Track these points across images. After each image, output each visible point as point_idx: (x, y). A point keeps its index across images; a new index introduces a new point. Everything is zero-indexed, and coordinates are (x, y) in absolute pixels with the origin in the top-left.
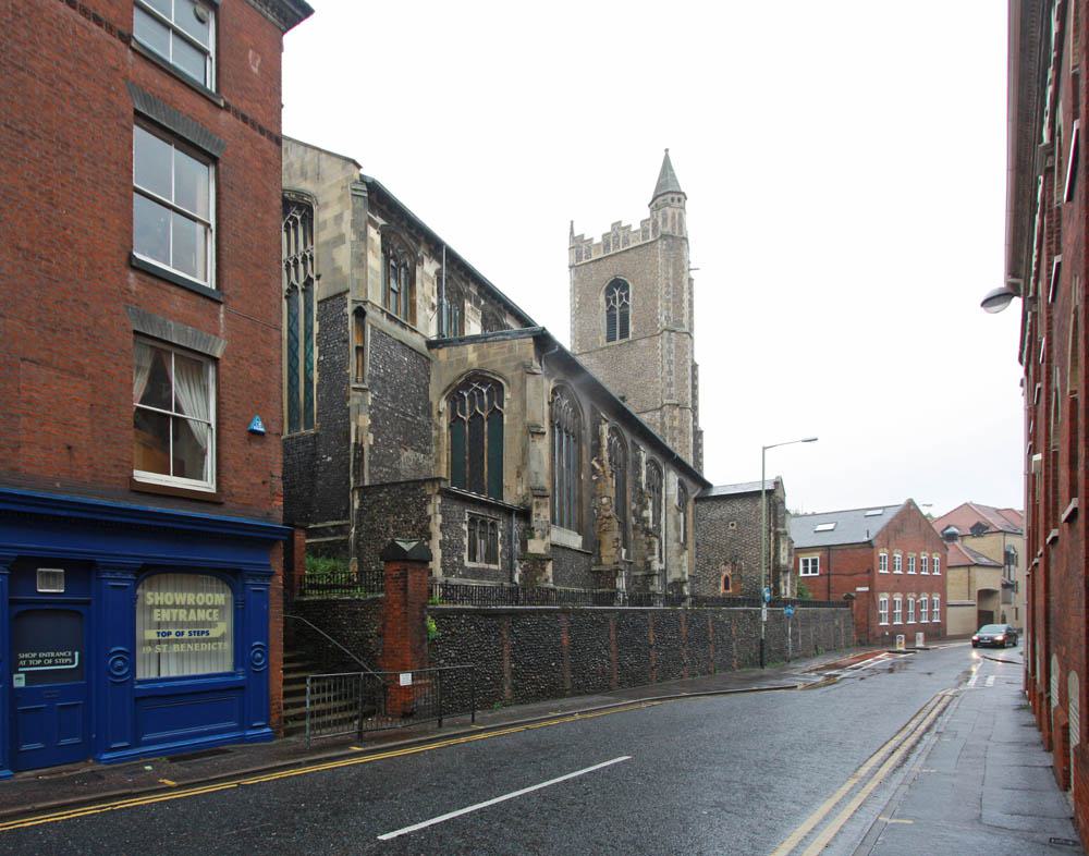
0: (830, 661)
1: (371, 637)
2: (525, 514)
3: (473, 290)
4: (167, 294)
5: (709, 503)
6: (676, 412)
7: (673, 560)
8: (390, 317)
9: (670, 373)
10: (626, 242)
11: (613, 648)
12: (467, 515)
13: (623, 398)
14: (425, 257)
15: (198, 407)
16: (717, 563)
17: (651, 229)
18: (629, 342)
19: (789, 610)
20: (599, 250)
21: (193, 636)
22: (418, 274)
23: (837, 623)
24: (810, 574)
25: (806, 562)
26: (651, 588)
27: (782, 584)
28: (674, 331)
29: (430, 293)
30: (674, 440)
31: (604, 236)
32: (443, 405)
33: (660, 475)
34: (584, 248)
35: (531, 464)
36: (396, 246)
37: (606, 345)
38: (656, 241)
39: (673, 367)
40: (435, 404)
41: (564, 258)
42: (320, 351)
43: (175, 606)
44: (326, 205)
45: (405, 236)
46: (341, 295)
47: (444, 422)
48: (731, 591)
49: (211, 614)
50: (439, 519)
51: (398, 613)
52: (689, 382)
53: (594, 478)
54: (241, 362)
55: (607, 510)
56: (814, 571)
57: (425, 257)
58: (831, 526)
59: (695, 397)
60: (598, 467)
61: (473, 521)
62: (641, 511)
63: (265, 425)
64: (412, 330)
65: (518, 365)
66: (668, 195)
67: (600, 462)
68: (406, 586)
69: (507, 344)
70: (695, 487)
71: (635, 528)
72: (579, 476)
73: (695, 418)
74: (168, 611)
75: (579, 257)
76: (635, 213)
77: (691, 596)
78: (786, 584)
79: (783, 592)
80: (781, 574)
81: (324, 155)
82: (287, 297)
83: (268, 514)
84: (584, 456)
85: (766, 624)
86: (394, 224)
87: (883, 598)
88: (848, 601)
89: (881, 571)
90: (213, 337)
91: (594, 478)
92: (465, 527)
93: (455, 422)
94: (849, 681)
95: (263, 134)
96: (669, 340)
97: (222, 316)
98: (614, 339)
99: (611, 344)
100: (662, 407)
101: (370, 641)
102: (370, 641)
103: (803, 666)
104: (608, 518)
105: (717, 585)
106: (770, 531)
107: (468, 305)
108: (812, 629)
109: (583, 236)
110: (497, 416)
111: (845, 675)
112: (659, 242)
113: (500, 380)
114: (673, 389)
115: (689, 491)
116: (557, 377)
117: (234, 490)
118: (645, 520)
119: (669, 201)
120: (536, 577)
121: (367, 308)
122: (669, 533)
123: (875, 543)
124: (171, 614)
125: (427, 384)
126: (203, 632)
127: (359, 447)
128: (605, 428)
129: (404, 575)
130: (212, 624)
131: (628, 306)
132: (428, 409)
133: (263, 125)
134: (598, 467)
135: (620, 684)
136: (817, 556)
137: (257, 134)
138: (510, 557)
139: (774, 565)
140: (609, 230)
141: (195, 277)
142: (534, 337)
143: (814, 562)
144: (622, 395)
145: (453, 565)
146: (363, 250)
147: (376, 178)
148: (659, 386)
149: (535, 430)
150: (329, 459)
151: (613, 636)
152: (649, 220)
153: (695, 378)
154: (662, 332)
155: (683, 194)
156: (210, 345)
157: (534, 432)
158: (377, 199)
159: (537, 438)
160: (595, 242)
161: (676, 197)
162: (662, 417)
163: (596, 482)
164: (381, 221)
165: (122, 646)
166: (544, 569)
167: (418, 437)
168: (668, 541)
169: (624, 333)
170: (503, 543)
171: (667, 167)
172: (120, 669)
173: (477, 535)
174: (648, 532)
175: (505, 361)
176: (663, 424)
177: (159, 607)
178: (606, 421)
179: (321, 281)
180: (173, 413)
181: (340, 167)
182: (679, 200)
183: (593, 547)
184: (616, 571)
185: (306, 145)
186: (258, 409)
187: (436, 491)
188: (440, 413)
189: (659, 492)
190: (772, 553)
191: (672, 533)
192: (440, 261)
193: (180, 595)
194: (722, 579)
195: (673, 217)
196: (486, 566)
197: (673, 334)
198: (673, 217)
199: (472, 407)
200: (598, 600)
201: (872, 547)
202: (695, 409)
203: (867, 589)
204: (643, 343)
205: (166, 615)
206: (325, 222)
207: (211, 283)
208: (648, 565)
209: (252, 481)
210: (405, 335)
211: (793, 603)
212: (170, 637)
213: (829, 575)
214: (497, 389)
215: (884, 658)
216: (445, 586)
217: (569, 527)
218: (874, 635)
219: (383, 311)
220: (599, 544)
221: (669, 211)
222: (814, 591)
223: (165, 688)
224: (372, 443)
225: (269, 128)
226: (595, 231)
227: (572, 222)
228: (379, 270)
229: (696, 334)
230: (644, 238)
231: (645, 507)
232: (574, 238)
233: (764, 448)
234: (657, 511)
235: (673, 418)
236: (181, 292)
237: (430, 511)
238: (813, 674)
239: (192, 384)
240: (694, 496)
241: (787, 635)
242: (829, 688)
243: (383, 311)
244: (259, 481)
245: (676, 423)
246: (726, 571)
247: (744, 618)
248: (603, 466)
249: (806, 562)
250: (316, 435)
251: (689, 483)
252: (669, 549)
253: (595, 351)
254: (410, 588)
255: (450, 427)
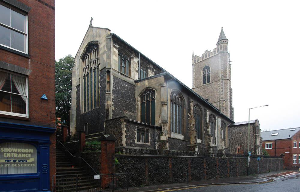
0: (273, 174)
1: (98, 164)
2: (160, 129)
3: (152, 67)
4: (7, 55)
5: (233, 127)
6: (224, 102)
7: (219, 144)
8: (121, 74)
9: (222, 91)
10: (209, 55)
11: (189, 168)
12: (136, 128)
13: (207, 100)
14: (134, 57)
15: (24, 92)
16: (235, 145)
17: (217, 50)
18: (210, 83)
19: (259, 159)
20: (201, 59)
21: (20, 162)
22: (132, 61)
23: (277, 163)
24: (269, 148)
25: (267, 145)
26: (210, 152)
27: (257, 151)
28: (224, 79)
29: (136, 68)
30: (223, 110)
31: (202, 55)
32: (139, 99)
33: (215, 119)
34: (197, 58)
35: (165, 113)
36: (124, 54)
37: (203, 85)
38: (218, 54)
39: (223, 90)
40: (137, 98)
41: (191, 62)
42: (100, 85)
43: (12, 152)
44: (102, 43)
45: (127, 51)
46: (105, 68)
47: (139, 104)
48: (240, 153)
49: (28, 155)
50: (125, 129)
51: (104, 157)
52: (229, 94)
53: (188, 119)
54: (38, 77)
55: (192, 128)
56: (270, 147)
57: (134, 57)
58: (277, 134)
59: (231, 98)
60: (189, 115)
61: (139, 130)
62: (207, 129)
63: (47, 97)
64: (129, 78)
65: (159, 85)
66: (223, 40)
67: (190, 114)
68: (106, 148)
69: (156, 79)
70: (228, 123)
71: (205, 134)
72: (183, 119)
73: (231, 104)
74: (10, 154)
75: (195, 62)
76: (212, 46)
77: (226, 154)
78: (258, 151)
79: (258, 153)
80: (257, 148)
81: (101, 30)
82: (93, 71)
83: (49, 125)
84: (185, 112)
85: (249, 162)
86: (123, 47)
87: (295, 155)
88: (282, 156)
89: (294, 147)
90: (26, 69)
91: (188, 119)
92: (136, 132)
93: (142, 104)
94: (278, 181)
95: (47, 6)
96: (222, 82)
97: (30, 62)
98: (205, 83)
99: (204, 85)
100: (220, 101)
101: (98, 165)
102: (98, 165)
103: (263, 176)
104: (192, 130)
105: (236, 151)
106: (253, 135)
107: (149, 71)
108: (268, 164)
109: (196, 55)
110: (153, 100)
111: (277, 179)
112: (219, 54)
113: (154, 90)
114: (223, 96)
115: (226, 124)
116: (173, 88)
117: (35, 117)
118: (208, 131)
119: (223, 42)
120: (163, 147)
121: (112, 71)
122: (218, 136)
123: (292, 139)
124: (11, 155)
125: (134, 93)
126: (24, 161)
127: (108, 110)
128: (192, 104)
129: (106, 145)
130: (29, 158)
131: (210, 74)
132: (134, 100)
133: (46, 3)
134: (189, 115)
135: (192, 180)
136: (271, 143)
137: (45, 6)
138: (154, 141)
139: (255, 145)
140: (204, 53)
141: (24, 52)
142: (164, 76)
143: (270, 145)
144: (207, 98)
145: (131, 143)
146: (110, 54)
147: (115, 33)
148: (219, 95)
149: (164, 103)
150: (102, 114)
151: (189, 165)
152: (216, 48)
153: (231, 93)
154: (220, 80)
155: (227, 39)
156: (25, 71)
157: (164, 104)
158: (116, 39)
159: (164, 106)
160: (200, 57)
161: (225, 41)
162: (220, 104)
163: (189, 120)
164: (118, 47)
165: (46, 164)
166: (166, 145)
167: (131, 107)
168: (218, 138)
169: (208, 81)
170: (151, 137)
171: (222, 32)
172: (45, 170)
173: (141, 134)
174: (209, 135)
175: (156, 84)
176: (220, 106)
177: (6, 152)
178: (192, 102)
179: (100, 65)
180: (11, 93)
181: (105, 32)
182: (226, 41)
183: (187, 139)
184: (195, 146)
185: (97, 28)
186: (45, 92)
187: (124, 120)
188: (138, 101)
189: (215, 124)
190: (254, 142)
191: (219, 136)
192: (138, 58)
193: (15, 149)
194: (237, 149)
195: (224, 47)
196: (144, 144)
197: (223, 80)
198: (224, 47)
199: (147, 98)
200: (189, 154)
201: (291, 140)
202: (231, 102)
203: (289, 153)
204: (214, 83)
205: (9, 155)
206: (101, 48)
207: (27, 53)
208: (209, 145)
209: (42, 114)
210: (127, 79)
211: (260, 156)
212: (11, 162)
213: (275, 148)
214: (153, 92)
215: (294, 174)
216: (126, 149)
217: (179, 133)
218: (291, 167)
219: (119, 72)
220: (190, 138)
221: (222, 45)
222: (270, 153)
223: (6, 177)
224: (114, 109)
225: (50, 4)
226: (200, 53)
227: (193, 52)
228: (118, 60)
229: (232, 80)
230: (215, 54)
231: (208, 128)
232: (194, 56)
233: (250, 109)
234: (214, 129)
235: (223, 104)
236: (12, 54)
237: (122, 126)
238: (265, 178)
239: (19, 84)
240: (228, 125)
241: (258, 166)
242: (268, 183)
243: (119, 72)
244: (46, 114)
245: (224, 105)
246: (239, 147)
247: (241, 161)
248: (191, 115)
249: (267, 145)
250: (100, 108)
251: (226, 121)
252: (218, 141)
253: (199, 87)
254: (108, 149)
255: (141, 105)
